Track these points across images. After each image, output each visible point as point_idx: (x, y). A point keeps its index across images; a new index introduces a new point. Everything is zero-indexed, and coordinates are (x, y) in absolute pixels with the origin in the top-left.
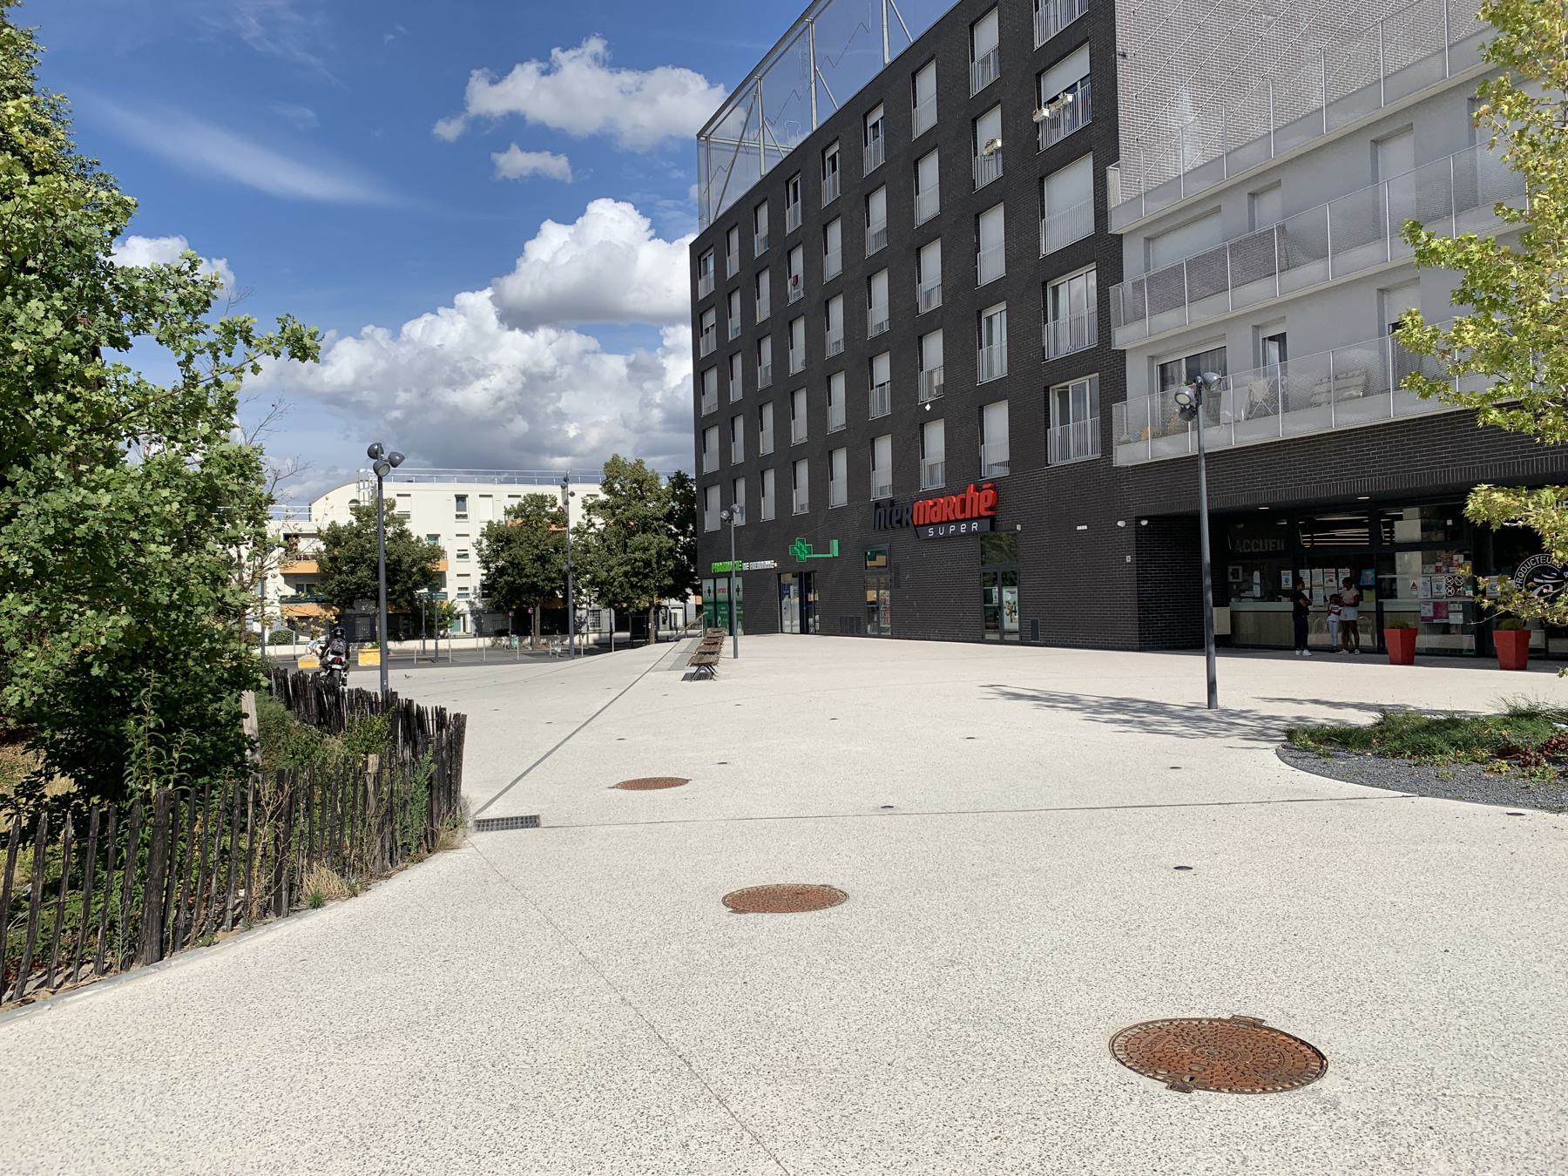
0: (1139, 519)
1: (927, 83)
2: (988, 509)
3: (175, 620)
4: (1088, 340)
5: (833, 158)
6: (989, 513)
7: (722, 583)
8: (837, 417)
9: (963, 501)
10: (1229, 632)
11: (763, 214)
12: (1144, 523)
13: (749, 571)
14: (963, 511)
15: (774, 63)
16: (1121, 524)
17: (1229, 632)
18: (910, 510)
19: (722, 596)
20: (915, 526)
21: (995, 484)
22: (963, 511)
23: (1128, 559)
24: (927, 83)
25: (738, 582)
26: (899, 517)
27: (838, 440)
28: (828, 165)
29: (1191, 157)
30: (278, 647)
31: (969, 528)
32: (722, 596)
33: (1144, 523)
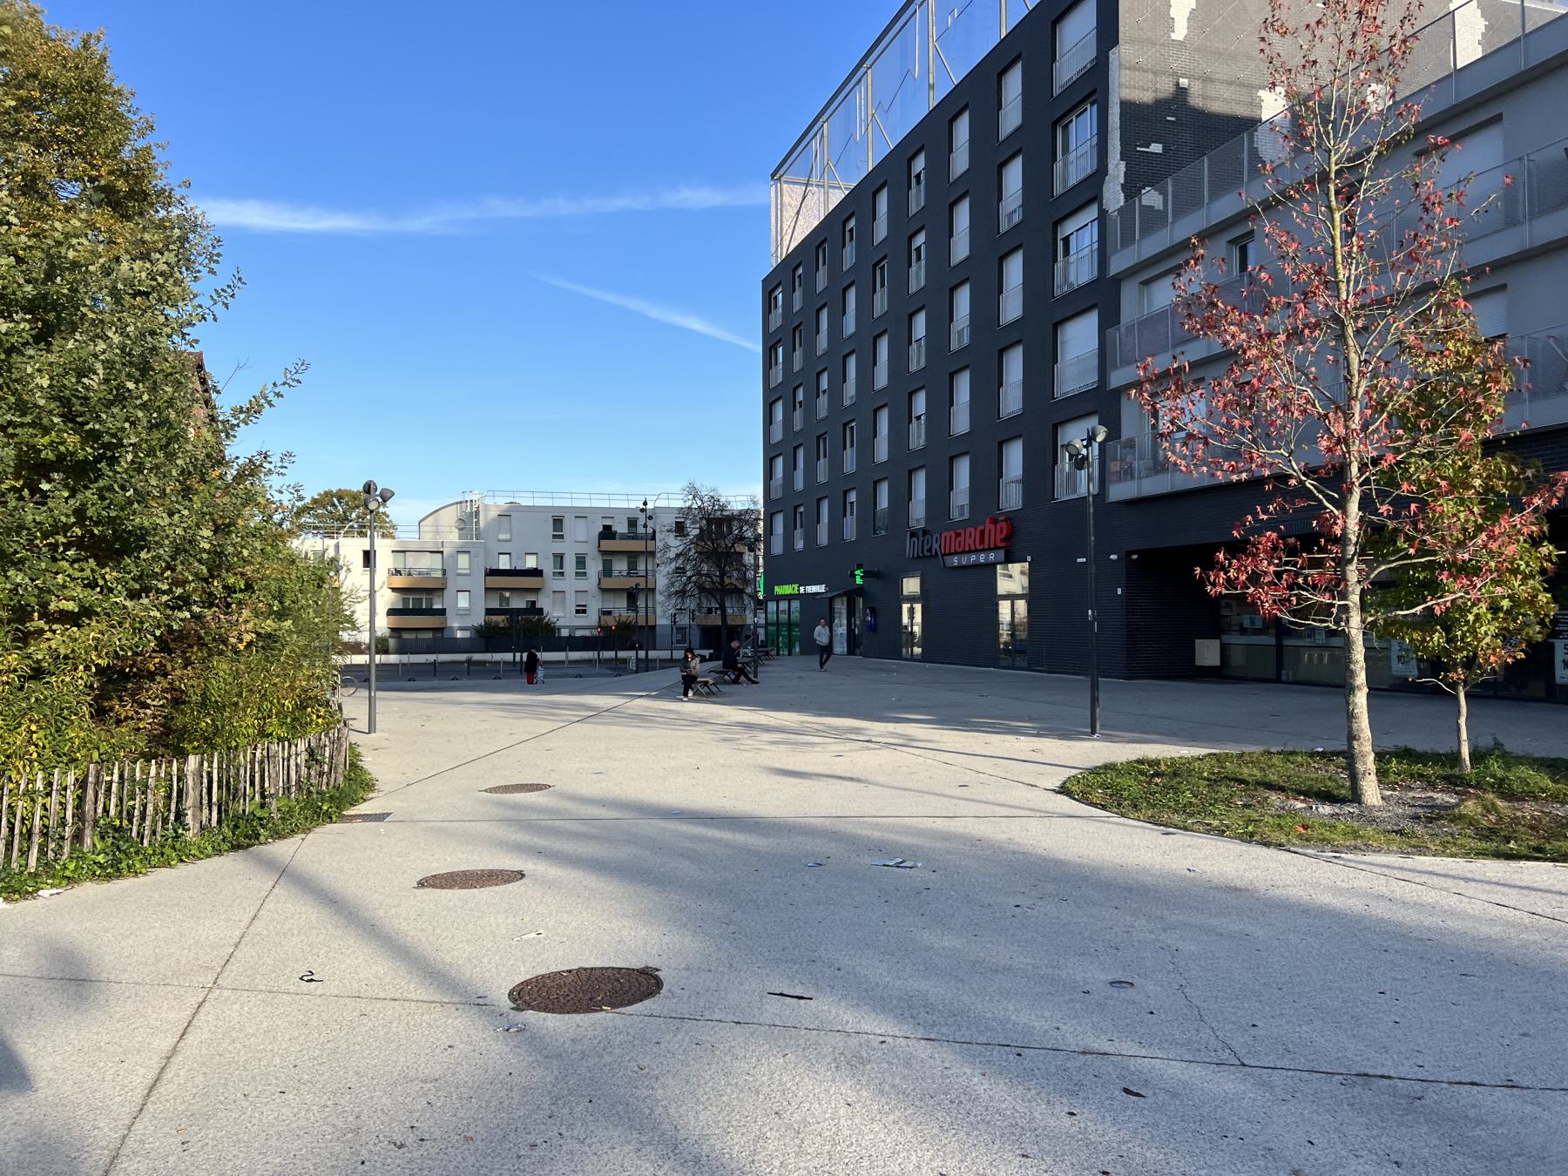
0: (1130, 553)
1: (1014, 84)
2: (1002, 540)
3: (49, 665)
4: (1090, 379)
5: (851, 230)
6: (1004, 544)
7: (783, 605)
8: (1012, 400)
9: (982, 532)
10: (1218, 664)
11: (883, 200)
12: (1135, 557)
13: (806, 594)
14: (982, 542)
15: (888, 46)
16: (1113, 557)
17: (1218, 664)
18: (973, 534)
19: (784, 617)
20: (943, 555)
21: (1010, 517)
22: (982, 542)
23: (1119, 591)
24: (1014, 84)
25: (796, 605)
26: (959, 539)
27: (963, 446)
28: (914, 181)
29: (1469, 49)
30: (411, 656)
31: (987, 558)
32: (784, 617)
33: (1135, 557)
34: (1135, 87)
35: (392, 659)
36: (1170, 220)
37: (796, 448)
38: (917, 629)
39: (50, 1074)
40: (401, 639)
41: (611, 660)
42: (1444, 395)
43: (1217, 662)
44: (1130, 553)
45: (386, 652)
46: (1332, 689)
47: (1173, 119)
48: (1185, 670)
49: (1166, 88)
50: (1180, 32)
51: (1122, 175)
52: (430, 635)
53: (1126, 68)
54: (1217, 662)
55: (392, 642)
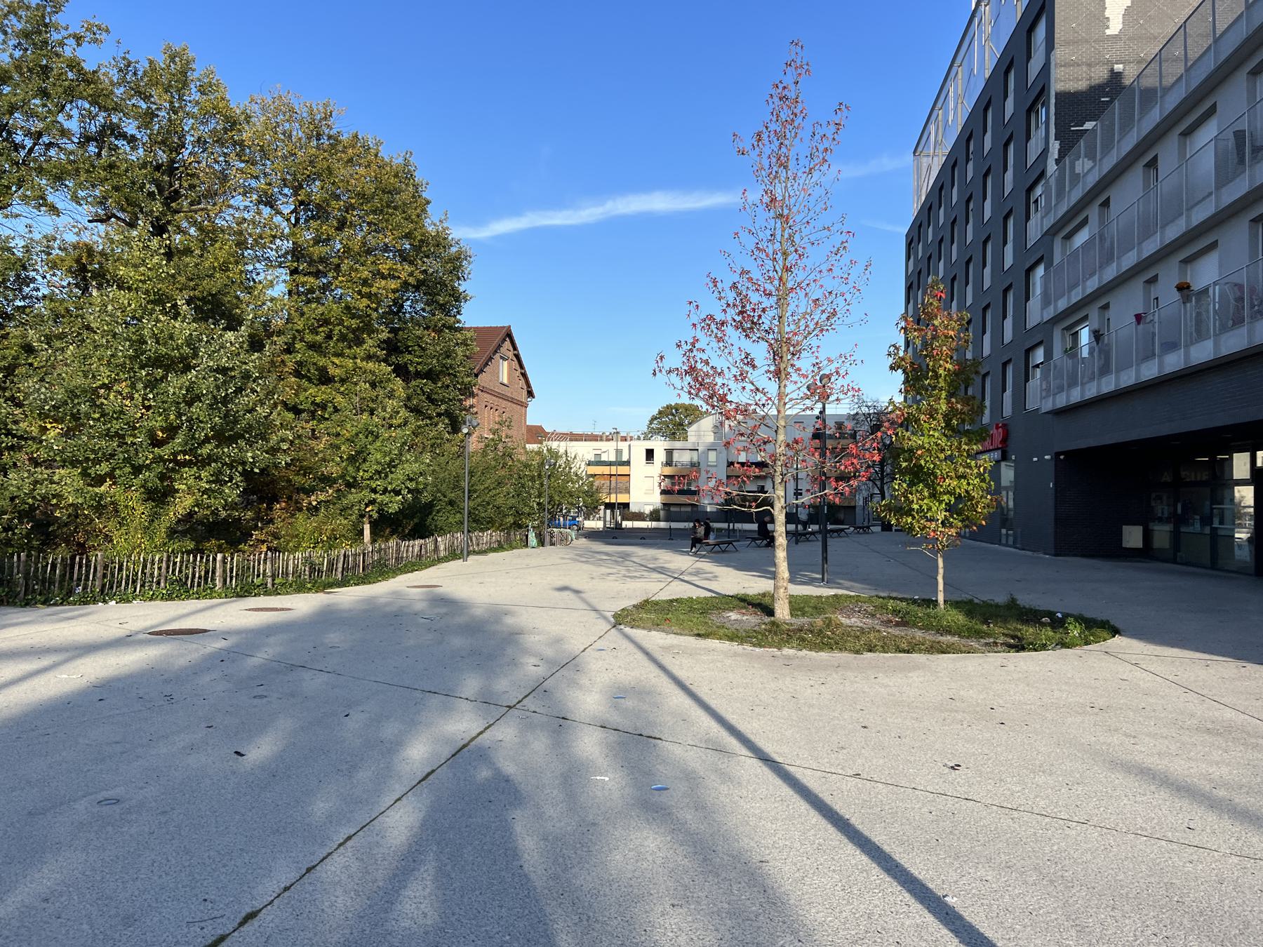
12: (1062, 457)
34: (1070, 80)
35: (662, 525)
36: (1067, 189)
37: (1005, 365)
38: (1011, 504)
39: (355, 781)
40: (668, 511)
41: (725, 530)
42: (251, 435)
43: (1140, 544)
44: (1058, 454)
45: (658, 520)
46: (1234, 575)
47: (1107, 99)
48: (1113, 551)
49: (1100, 75)
50: (1115, 27)
51: (1057, 152)
52: (689, 509)
53: (1061, 66)
54: (1140, 544)
55: (662, 513)
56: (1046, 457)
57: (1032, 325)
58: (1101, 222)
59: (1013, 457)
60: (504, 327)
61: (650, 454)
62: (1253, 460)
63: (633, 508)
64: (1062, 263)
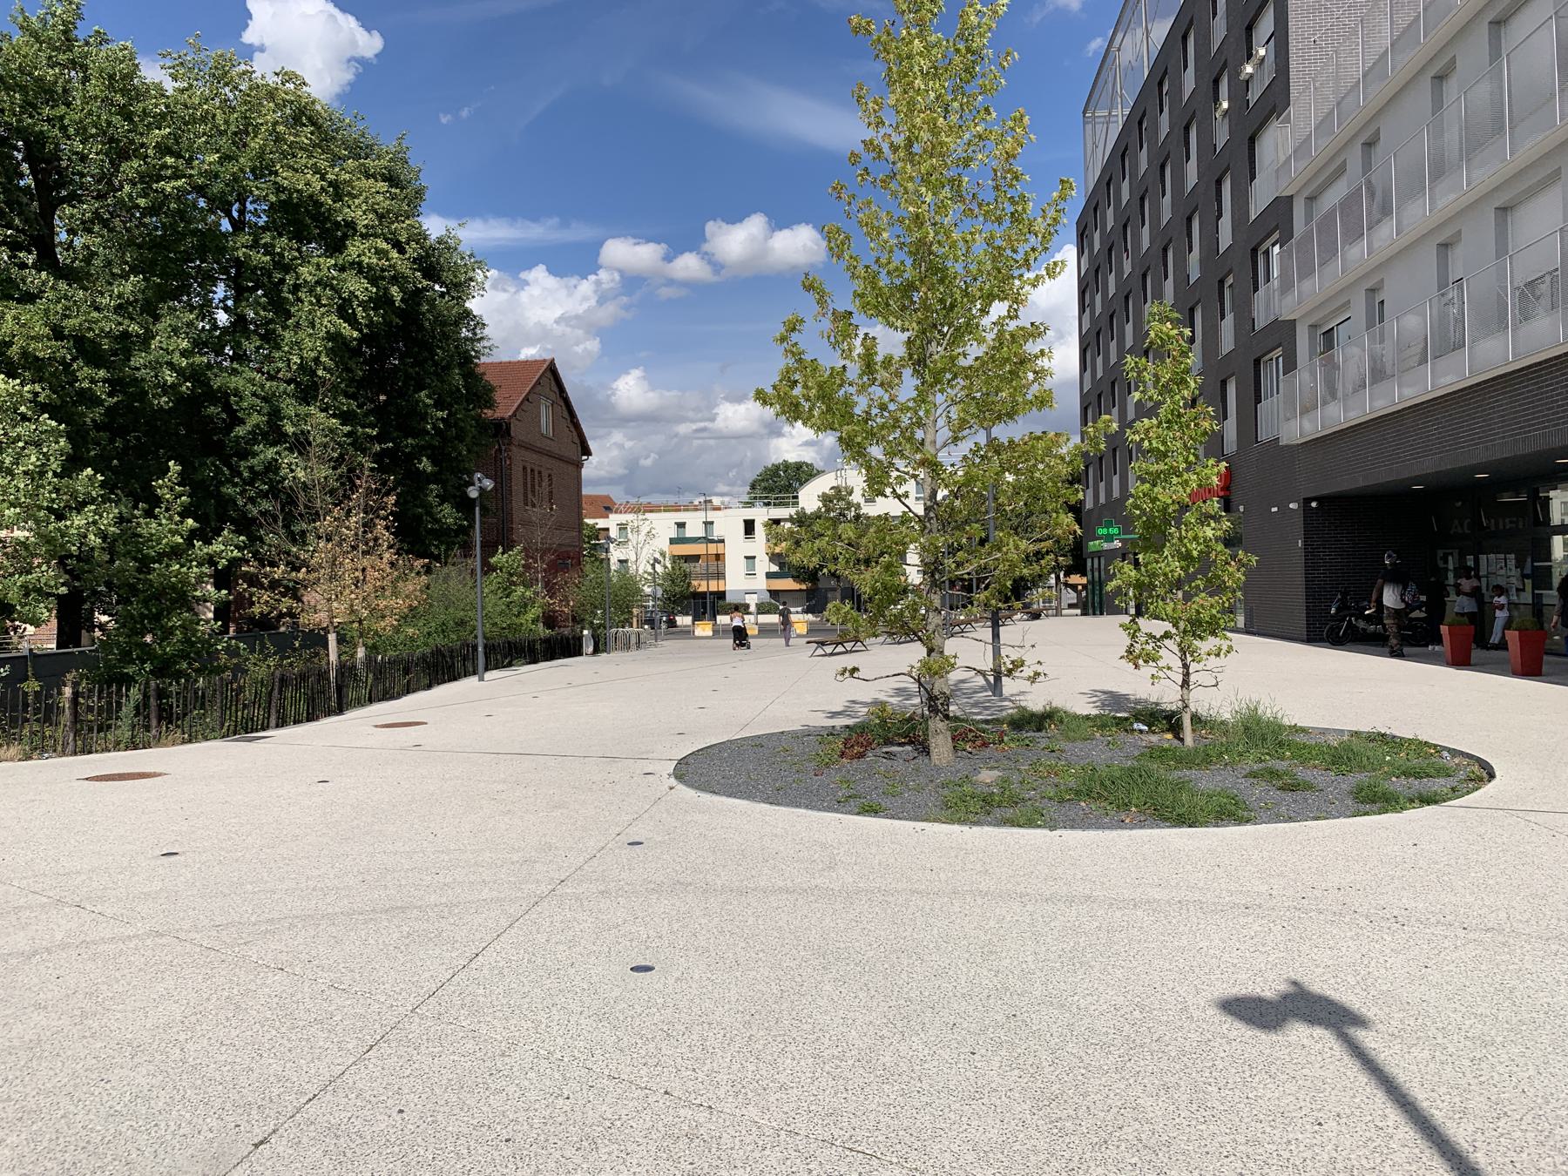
12: (1314, 504)
44: (1308, 501)
56: (1291, 506)
57: (1262, 325)
58: (1367, 166)
59: (1241, 508)
60: (545, 361)
61: (749, 527)
62: (754, 637)
63: (729, 599)
64: (1308, 236)
